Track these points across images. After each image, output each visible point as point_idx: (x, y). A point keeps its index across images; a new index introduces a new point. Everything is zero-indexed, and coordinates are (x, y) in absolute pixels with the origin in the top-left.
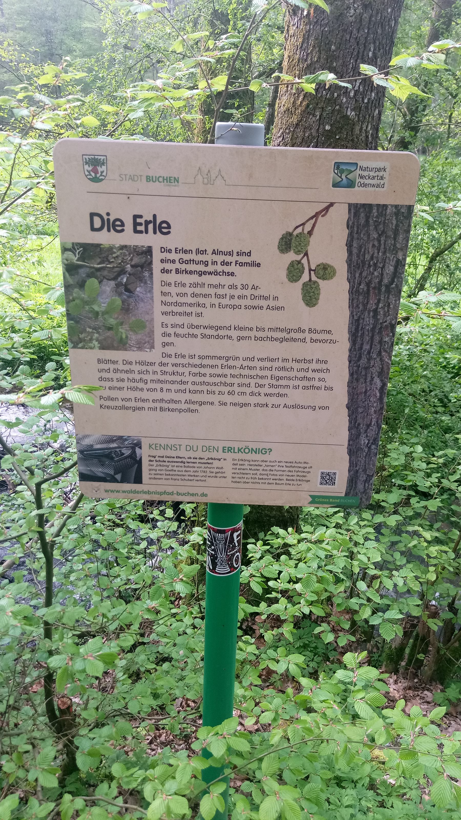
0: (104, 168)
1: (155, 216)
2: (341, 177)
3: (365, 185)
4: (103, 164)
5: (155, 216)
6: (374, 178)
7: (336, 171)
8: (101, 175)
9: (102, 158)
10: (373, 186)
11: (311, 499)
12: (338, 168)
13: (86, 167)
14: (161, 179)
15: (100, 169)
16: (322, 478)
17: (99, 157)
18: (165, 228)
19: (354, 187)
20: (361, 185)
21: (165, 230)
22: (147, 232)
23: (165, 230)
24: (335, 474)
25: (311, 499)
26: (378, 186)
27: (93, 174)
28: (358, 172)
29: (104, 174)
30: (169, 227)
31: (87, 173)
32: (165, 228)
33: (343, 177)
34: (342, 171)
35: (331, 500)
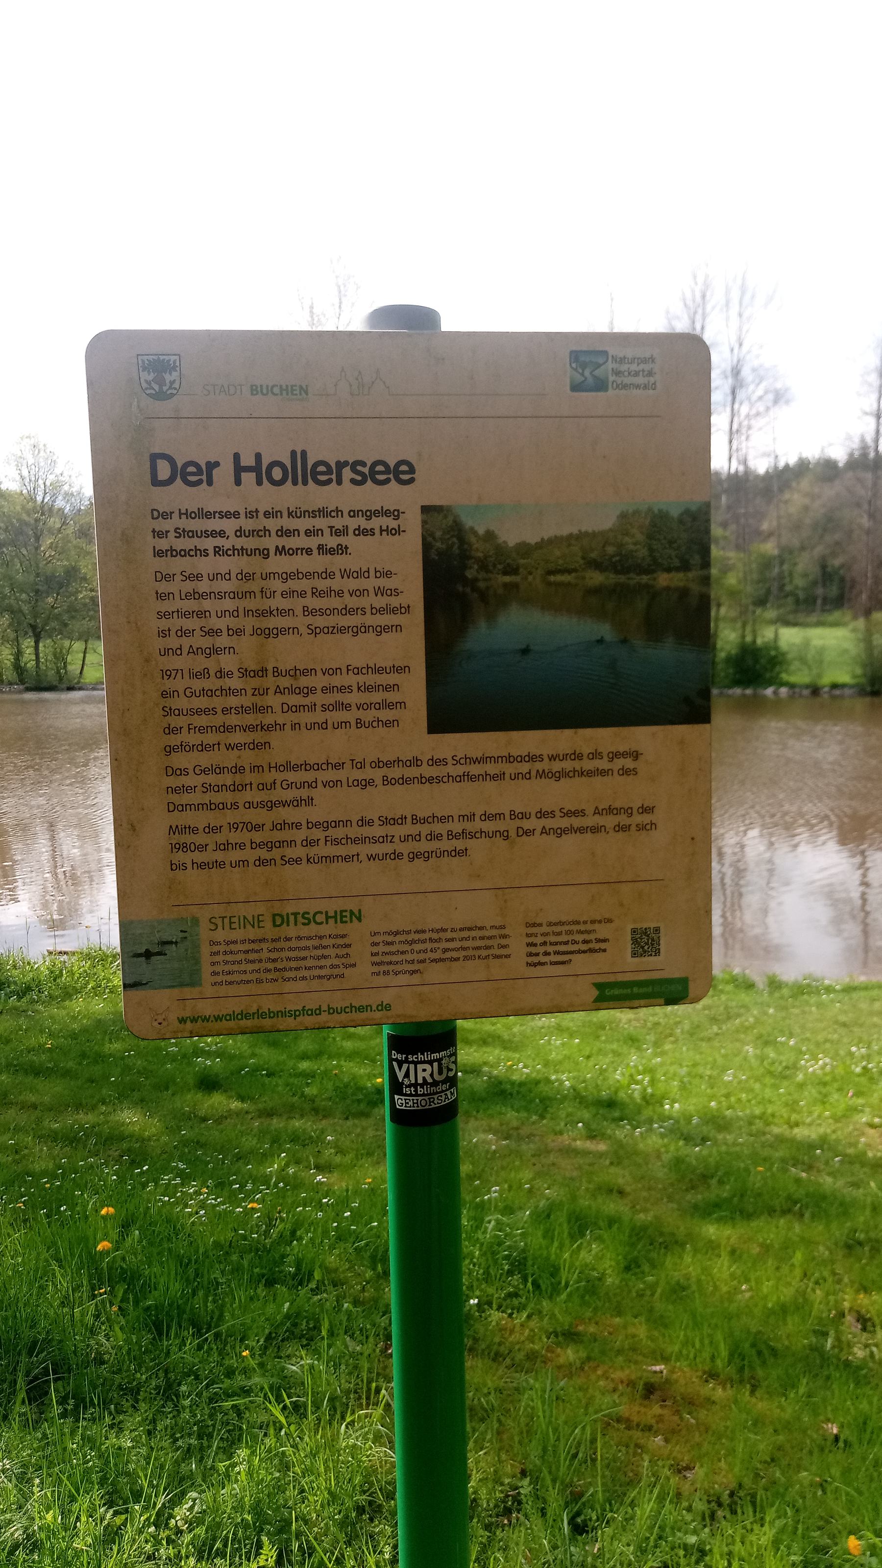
0: (175, 375)
1: (258, 457)
2: (582, 374)
3: (625, 386)
4: (174, 368)
5: (258, 457)
6: (637, 374)
7: (574, 365)
8: (170, 388)
9: (173, 358)
10: (638, 387)
11: (595, 993)
12: (576, 360)
13: (145, 376)
14: (276, 390)
15: (168, 378)
16: (635, 941)
17: (167, 358)
18: (404, 472)
19: (606, 390)
20: (618, 386)
21: (405, 477)
22: (339, 482)
23: (405, 477)
24: (657, 930)
25: (595, 993)
26: (645, 387)
27: (156, 387)
28: (610, 365)
29: (176, 385)
30: (412, 470)
31: (144, 385)
32: (404, 472)
33: (587, 373)
34: (584, 366)
35: (635, 990)
